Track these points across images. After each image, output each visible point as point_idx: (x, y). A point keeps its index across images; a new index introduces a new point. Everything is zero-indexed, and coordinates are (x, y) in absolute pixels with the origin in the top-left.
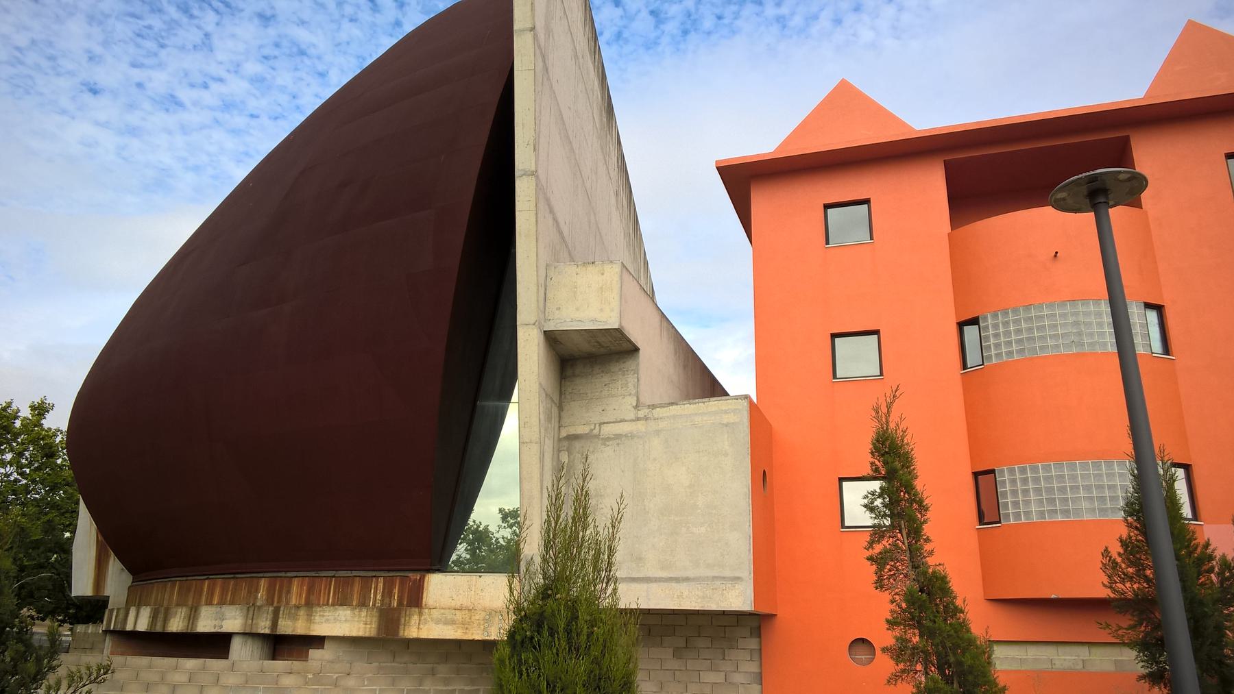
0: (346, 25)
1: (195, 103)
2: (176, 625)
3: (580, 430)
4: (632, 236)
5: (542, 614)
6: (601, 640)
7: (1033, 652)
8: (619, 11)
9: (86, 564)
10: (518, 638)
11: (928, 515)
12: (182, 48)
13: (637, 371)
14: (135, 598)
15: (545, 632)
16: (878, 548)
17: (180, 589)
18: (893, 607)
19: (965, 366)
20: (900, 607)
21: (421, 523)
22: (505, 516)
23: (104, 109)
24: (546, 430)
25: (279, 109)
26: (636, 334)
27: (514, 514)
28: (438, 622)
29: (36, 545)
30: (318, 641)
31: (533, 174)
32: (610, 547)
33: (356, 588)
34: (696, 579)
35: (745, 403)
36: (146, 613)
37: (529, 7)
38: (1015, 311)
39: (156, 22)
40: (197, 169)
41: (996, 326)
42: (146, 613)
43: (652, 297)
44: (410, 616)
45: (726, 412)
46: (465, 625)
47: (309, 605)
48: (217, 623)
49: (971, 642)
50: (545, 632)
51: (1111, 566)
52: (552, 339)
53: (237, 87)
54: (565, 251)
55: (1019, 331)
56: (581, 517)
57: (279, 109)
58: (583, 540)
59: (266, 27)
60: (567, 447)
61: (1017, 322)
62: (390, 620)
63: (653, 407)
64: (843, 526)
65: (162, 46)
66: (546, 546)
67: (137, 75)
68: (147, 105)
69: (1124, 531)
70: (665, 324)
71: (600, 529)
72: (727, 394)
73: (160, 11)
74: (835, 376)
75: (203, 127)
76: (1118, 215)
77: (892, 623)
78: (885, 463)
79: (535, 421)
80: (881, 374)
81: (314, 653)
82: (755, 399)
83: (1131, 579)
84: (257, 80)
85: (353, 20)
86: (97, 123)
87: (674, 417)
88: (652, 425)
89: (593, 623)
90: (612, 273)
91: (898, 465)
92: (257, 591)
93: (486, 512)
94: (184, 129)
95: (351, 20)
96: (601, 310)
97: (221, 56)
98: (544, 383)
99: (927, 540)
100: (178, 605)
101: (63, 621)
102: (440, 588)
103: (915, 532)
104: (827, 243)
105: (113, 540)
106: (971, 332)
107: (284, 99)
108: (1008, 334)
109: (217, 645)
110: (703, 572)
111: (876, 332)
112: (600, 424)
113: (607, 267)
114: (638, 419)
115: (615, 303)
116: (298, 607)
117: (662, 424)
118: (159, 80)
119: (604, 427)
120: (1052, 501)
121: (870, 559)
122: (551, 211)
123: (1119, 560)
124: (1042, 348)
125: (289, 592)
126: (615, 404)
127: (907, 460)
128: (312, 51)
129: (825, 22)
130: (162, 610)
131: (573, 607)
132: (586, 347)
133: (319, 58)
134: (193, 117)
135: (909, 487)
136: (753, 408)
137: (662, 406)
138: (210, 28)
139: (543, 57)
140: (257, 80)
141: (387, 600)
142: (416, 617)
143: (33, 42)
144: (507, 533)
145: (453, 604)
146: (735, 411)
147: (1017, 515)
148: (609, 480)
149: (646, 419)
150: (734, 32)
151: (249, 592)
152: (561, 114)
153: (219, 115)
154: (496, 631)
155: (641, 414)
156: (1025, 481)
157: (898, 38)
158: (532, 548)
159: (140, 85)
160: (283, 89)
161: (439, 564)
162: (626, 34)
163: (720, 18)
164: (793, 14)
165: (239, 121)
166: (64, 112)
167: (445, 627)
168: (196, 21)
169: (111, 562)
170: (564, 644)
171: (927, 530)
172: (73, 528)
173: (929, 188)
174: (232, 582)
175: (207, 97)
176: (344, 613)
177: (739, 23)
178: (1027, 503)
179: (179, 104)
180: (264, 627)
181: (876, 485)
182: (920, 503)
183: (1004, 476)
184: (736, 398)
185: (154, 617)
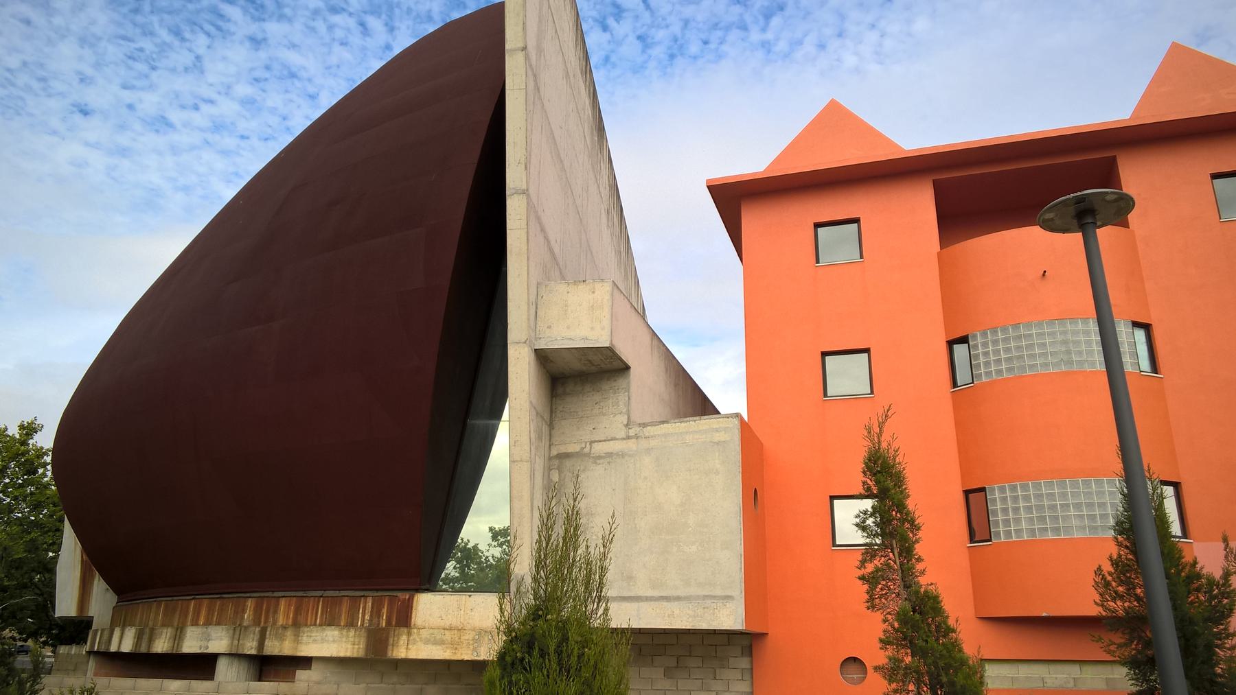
0: (337, 48)
1: (186, 125)
2: (161, 645)
3: (572, 448)
4: (623, 254)
5: (532, 635)
6: (592, 662)
7: (1024, 671)
8: (607, 36)
9: (70, 585)
10: (508, 659)
11: (920, 534)
12: (173, 70)
13: (628, 390)
14: (119, 619)
15: (536, 653)
16: (870, 568)
17: (164, 614)
18: (885, 626)
19: (955, 384)
20: (892, 626)
21: (412, 543)
22: (496, 534)
23: (94, 130)
24: (536, 448)
25: (269, 131)
26: (626, 352)
27: (504, 532)
28: (427, 642)
29: (19, 564)
30: (306, 662)
31: (525, 192)
32: (601, 568)
33: (345, 608)
34: (688, 598)
35: (736, 421)
36: (130, 634)
37: (520, 28)
38: (1005, 330)
39: (147, 45)
40: (186, 189)
41: (985, 345)
42: (130, 634)
43: (643, 315)
44: (399, 636)
45: (717, 430)
46: (454, 645)
47: (297, 625)
48: (203, 643)
49: (963, 662)
50: (536, 653)
51: (1103, 585)
52: (543, 357)
53: (227, 108)
54: (556, 269)
55: (1008, 350)
56: (572, 536)
57: (269, 131)
58: (574, 561)
59: (257, 50)
60: (557, 467)
61: (1006, 340)
62: (378, 641)
63: (644, 425)
64: (834, 544)
65: (154, 68)
66: (537, 566)
67: (128, 96)
68: (138, 126)
69: (1114, 550)
70: (656, 342)
71: (591, 550)
72: (718, 413)
73: (152, 34)
74: (825, 395)
75: (193, 148)
76: (1105, 235)
77: (885, 643)
78: (877, 482)
79: (525, 439)
80: (872, 393)
81: (301, 674)
82: (746, 417)
83: (1121, 597)
84: (248, 102)
85: (343, 44)
86: (87, 144)
87: (665, 435)
88: (643, 444)
89: (584, 644)
90: (603, 291)
91: (890, 484)
92: (244, 611)
93: (475, 531)
94: (175, 150)
95: (342, 44)
96: (592, 329)
97: (211, 78)
98: (534, 401)
99: (919, 560)
100: (163, 625)
101: (45, 643)
102: (430, 607)
103: (907, 552)
104: (818, 262)
105: (99, 559)
106: (960, 350)
107: (274, 121)
108: (997, 352)
109: (202, 666)
110: (693, 591)
111: (866, 351)
112: (592, 442)
113: (598, 285)
114: (629, 438)
115: (606, 322)
116: (285, 628)
117: (653, 443)
118: (149, 102)
119: (595, 445)
120: (1042, 519)
121: (862, 578)
122: (543, 230)
123: (1109, 578)
124: (1031, 366)
125: (276, 612)
126: (606, 423)
127: (899, 480)
128: (303, 74)
129: (809, 47)
130: (147, 630)
131: (563, 626)
132: (577, 365)
133: (310, 80)
134: (183, 138)
135: (901, 507)
136: (744, 425)
137: (652, 424)
138: (201, 51)
139: (535, 76)
140: (248, 102)
141: (375, 621)
142: (404, 637)
143: (25, 64)
144: (497, 552)
145: (442, 624)
146: (726, 429)
147: (1008, 533)
148: (600, 498)
149: (637, 437)
150: (720, 57)
151: (236, 612)
152: (552, 133)
153: (209, 137)
154: (487, 651)
155: (632, 432)
156: (1015, 499)
157: (881, 63)
158: (523, 567)
159: (130, 107)
160: (273, 111)
161: (428, 581)
162: (613, 59)
163: (706, 43)
164: (777, 39)
165: (229, 142)
166: (55, 133)
167: (434, 647)
168: (188, 44)
169: (96, 582)
170: (554, 666)
171: (919, 549)
172: (56, 546)
173: (918, 207)
174: (218, 602)
175: (198, 119)
176: (332, 633)
177: (724, 48)
178: (1017, 521)
179: (170, 125)
180: (250, 647)
181: (868, 504)
182: (912, 522)
183: (995, 494)
184: (728, 416)
185: (139, 638)
